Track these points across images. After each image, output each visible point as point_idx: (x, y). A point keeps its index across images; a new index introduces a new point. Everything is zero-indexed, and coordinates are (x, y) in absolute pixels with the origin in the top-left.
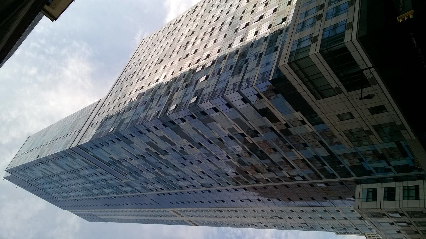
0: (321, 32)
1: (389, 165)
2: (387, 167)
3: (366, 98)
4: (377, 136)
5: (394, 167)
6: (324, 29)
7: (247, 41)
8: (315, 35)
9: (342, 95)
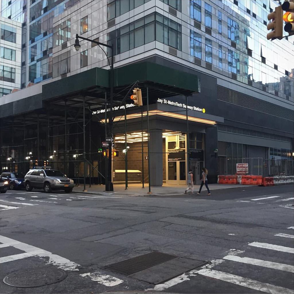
0: (179, 22)
1: (38, 61)
2: (36, 58)
3: (77, 41)
4: (60, 53)
5: (35, 65)
6: (180, 25)
7: (284, 266)
8: (178, 14)
9: (106, 27)
